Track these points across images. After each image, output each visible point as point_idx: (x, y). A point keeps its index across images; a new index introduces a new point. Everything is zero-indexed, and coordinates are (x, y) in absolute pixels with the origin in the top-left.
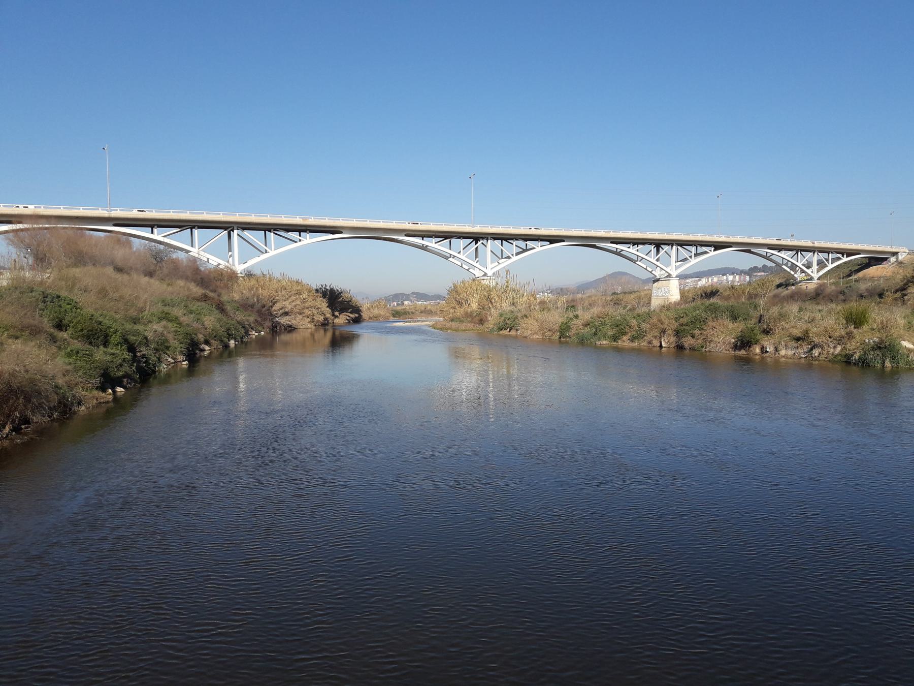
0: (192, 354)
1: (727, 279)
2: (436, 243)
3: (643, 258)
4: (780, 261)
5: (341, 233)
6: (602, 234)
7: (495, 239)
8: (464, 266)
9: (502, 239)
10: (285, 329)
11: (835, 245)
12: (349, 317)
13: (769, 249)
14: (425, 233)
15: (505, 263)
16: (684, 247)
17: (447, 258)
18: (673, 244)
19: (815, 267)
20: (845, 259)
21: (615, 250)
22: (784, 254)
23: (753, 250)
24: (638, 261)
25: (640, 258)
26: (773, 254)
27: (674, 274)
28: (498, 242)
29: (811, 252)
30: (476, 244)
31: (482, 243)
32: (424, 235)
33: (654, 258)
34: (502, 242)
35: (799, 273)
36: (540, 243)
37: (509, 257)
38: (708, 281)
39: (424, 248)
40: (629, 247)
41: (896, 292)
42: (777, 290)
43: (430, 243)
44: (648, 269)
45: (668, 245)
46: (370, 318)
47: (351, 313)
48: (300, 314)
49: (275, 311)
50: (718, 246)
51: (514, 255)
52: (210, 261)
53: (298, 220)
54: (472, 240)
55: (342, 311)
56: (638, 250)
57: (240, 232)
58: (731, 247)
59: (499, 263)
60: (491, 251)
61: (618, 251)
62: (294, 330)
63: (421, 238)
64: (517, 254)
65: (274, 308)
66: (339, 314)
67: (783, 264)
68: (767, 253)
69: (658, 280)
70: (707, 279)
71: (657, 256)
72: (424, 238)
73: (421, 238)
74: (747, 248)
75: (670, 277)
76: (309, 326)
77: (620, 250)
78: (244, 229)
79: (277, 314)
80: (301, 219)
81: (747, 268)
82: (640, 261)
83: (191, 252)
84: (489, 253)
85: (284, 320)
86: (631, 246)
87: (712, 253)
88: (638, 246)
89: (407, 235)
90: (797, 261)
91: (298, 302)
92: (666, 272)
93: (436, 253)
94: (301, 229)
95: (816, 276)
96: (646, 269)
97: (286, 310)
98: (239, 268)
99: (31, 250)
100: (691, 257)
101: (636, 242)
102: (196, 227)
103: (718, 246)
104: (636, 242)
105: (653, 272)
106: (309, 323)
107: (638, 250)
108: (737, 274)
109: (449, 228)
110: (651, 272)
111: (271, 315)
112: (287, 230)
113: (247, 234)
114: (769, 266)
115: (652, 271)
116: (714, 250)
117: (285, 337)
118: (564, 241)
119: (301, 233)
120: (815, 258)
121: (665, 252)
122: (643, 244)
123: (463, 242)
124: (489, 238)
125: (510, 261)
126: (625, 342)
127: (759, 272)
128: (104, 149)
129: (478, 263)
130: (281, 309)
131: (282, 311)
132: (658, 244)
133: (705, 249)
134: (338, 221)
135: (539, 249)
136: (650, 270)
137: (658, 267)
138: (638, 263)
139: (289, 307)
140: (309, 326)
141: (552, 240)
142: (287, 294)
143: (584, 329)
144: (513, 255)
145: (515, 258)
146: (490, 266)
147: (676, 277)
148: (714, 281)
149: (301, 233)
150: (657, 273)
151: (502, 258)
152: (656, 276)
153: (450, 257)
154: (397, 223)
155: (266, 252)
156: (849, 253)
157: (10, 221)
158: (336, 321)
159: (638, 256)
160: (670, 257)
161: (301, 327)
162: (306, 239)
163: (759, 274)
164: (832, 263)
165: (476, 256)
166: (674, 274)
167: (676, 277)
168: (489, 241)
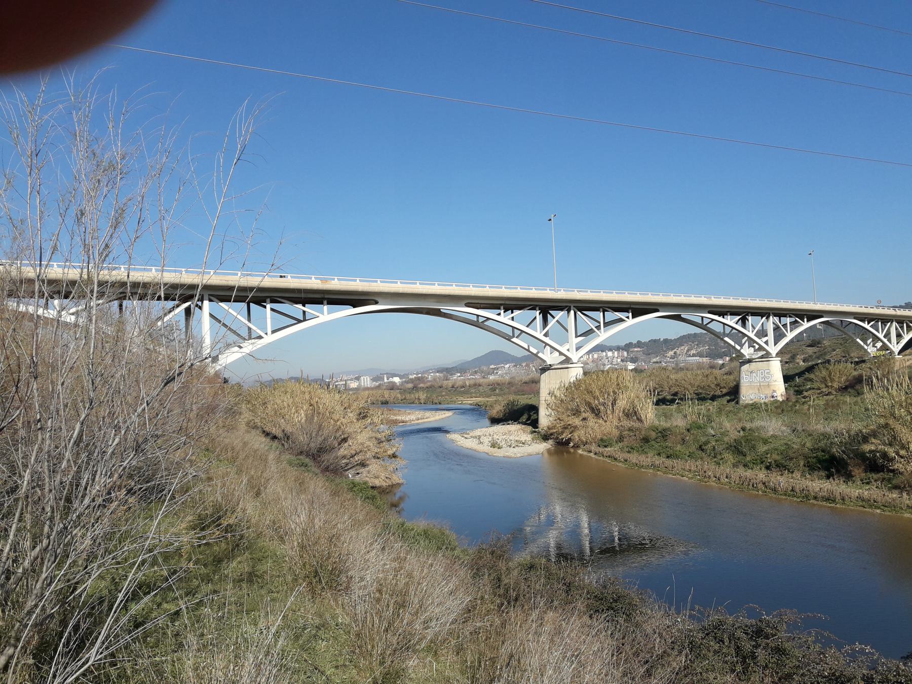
1: (606, 355)
3: (522, 331)
24: (513, 336)
25: (517, 332)
26: (488, 319)
28: (233, 311)
29: (562, 310)
33: (540, 333)
37: (260, 337)
38: (589, 358)
40: (499, 314)
50: (639, 309)
51: (269, 332)
53: (313, 283)
56: (513, 319)
57: (276, 306)
64: (273, 332)
67: (725, 335)
68: (702, 318)
71: (543, 330)
75: (568, 363)
80: (319, 281)
81: (623, 344)
82: (516, 337)
86: (502, 312)
88: (512, 313)
92: (561, 354)
100: (598, 328)
102: (325, 302)
103: (639, 309)
105: (540, 355)
108: (615, 351)
114: (662, 340)
115: (538, 353)
116: (633, 317)
120: (770, 323)
121: (557, 321)
127: (635, 348)
132: (546, 308)
136: (535, 351)
137: (548, 347)
138: (514, 340)
144: (266, 334)
151: (250, 338)
152: (544, 361)
155: (250, 335)
159: (513, 328)
160: (567, 330)
163: (636, 349)
164: (907, 334)
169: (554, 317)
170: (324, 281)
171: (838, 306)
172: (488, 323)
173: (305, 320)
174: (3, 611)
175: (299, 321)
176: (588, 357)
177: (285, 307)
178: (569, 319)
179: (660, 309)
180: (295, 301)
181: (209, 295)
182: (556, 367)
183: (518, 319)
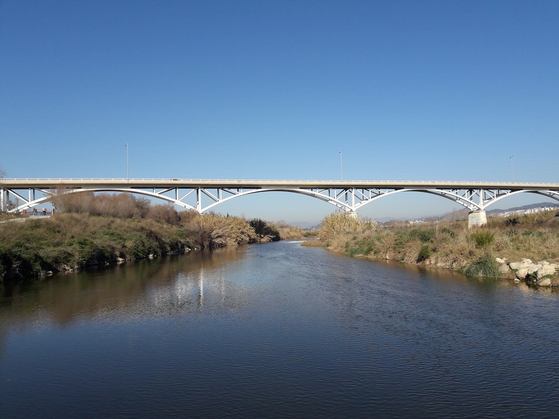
0: (102, 264)
2: (319, 192)
3: (460, 198)
5: (260, 188)
6: (430, 183)
7: (357, 188)
8: (338, 205)
9: (363, 189)
10: (219, 246)
12: (270, 237)
13: (550, 190)
14: (313, 187)
15: (364, 203)
16: (489, 190)
17: (327, 201)
18: (480, 189)
21: (441, 193)
23: (539, 191)
24: (457, 200)
25: (458, 199)
26: (554, 194)
27: (482, 208)
28: (360, 191)
30: (346, 191)
31: (349, 191)
32: (312, 187)
34: (498, 190)
36: (387, 190)
37: (367, 200)
38: (531, 211)
39: (313, 195)
40: (450, 192)
42: (555, 218)
43: (316, 192)
44: (465, 205)
45: (477, 189)
46: (287, 238)
47: (271, 235)
48: (229, 237)
49: (213, 235)
51: (370, 198)
52: (186, 207)
53: (235, 182)
54: (468, 190)
55: (265, 234)
57: (202, 190)
58: (522, 190)
59: (361, 203)
60: (355, 195)
61: (443, 194)
62: (225, 246)
64: (372, 198)
65: (212, 234)
66: (264, 236)
68: (550, 193)
69: (472, 212)
70: (530, 210)
72: (313, 190)
73: (311, 189)
74: (535, 190)
75: (480, 210)
76: (234, 244)
77: (444, 193)
78: (205, 188)
79: (214, 237)
82: (459, 200)
83: (175, 202)
84: (353, 196)
85: (218, 241)
87: (509, 194)
88: (457, 190)
89: (301, 188)
90: (176, 199)
91: (228, 230)
93: (453, 199)
96: (463, 205)
97: (219, 235)
98: (200, 210)
99: (54, 204)
101: (454, 188)
104: (454, 188)
105: (469, 207)
106: (234, 242)
107: (457, 192)
109: (298, 183)
110: (467, 207)
111: (211, 237)
112: (230, 188)
113: (206, 190)
115: (468, 206)
116: (510, 192)
117: (218, 251)
119: (239, 189)
121: (476, 193)
122: (460, 189)
123: (336, 192)
124: (353, 188)
125: (367, 202)
126: (371, 256)
128: (126, 146)
129: (347, 204)
131: (217, 235)
132: (471, 189)
133: (503, 191)
134: (299, 182)
136: (466, 206)
138: (457, 201)
139: (221, 233)
140: (234, 244)
141: (513, 189)
142: (222, 225)
143: (355, 246)
144: (369, 198)
145: (370, 200)
147: (484, 210)
148: (536, 211)
149: (239, 189)
150: (471, 208)
151: (363, 200)
152: (470, 210)
153: (329, 200)
154: (404, 182)
157: (48, 187)
158: (262, 240)
159: (457, 197)
160: (479, 196)
161: (229, 244)
162: (241, 193)
165: (346, 199)
167: (484, 210)
168: (353, 190)
169: (474, 192)
172: (445, 195)
173: (380, 194)
175: (378, 195)
176: (530, 212)
177: (374, 190)
179: (404, 188)
180: (377, 188)
181: (3, 188)
182: (475, 212)
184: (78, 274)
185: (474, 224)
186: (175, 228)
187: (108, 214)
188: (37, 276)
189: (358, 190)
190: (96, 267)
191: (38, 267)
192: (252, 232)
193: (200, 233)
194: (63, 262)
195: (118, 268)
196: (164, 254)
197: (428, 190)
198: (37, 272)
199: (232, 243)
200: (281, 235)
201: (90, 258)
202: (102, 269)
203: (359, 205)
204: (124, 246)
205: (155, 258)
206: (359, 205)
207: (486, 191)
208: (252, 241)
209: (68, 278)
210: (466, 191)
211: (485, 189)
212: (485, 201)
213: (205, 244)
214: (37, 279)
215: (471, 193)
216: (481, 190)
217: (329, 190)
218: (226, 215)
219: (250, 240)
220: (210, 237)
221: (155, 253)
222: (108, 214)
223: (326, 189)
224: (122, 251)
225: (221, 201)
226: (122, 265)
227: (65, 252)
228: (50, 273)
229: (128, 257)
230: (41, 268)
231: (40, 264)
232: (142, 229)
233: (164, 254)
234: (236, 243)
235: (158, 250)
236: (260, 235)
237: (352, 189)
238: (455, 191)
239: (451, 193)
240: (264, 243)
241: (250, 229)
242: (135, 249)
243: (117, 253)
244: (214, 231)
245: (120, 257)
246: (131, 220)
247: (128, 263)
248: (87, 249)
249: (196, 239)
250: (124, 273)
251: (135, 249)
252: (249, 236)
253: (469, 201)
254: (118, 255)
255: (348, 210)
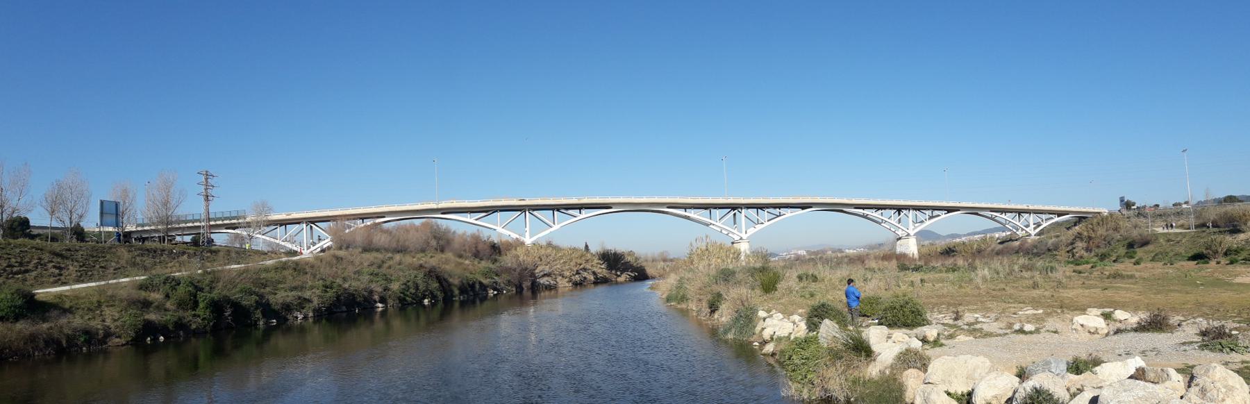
4: (1004, 221)
6: (434, 206)
7: (748, 208)
8: (723, 231)
9: (757, 208)
11: (1047, 208)
12: (629, 275)
15: (759, 227)
19: (1032, 226)
20: (1057, 219)
22: (470, 218)
27: (912, 233)
28: (752, 212)
32: (686, 207)
35: (1020, 230)
36: (789, 210)
37: (762, 223)
39: (865, 217)
41: (1067, 246)
43: (692, 213)
44: (892, 229)
45: (906, 209)
47: (631, 272)
60: (745, 216)
63: (684, 210)
64: (768, 221)
65: (536, 271)
69: (900, 239)
74: (974, 211)
76: (567, 285)
78: (534, 210)
84: (743, 218)
85: (544, 281)
87: (943, 215)
94: (580, 207)
95: (1033, 233)
98: (528, 241)
113: (535, 213)
118: (811, 207)
120: (1032, 219)
122: (885, 209)
123: (717, 213)
125: (763, 226)
130: (541, 271)
131: (542, 273)
132: (899, 209)
135: (943, 216)
136: (894, 230)
138: (883, 224)
139: (547, 269)
144: (926, 220)
145: (767, 224)
146: (911, 226)
150: (900, 233)
156: (1060, 214)
158: (619, 279)
165: (735, 223)
166: (912, 233)
170: (579, 199)
171: (515, 201)
173: (780, 216)
174: (216, 402)
175: (778, 216)
177: (771, 210)
178: (911, 213)
180: (775, 208)
183: (1008, 217)
184: (315, 322)
185: (799, 252)
186: (485, 264)
187: (387, 250)
188: (256, 324)
189: (749, 210)
190: (344, 315)
191: (258, 314)
192: (602, 270)
193: (518, 270)
194: (296, 309)
195: (377, 317)
196: (448, 300)
197: (845, 209)
198: (256, 322)
199: (563, 284)
200: (650, 271)
201: (331, 304)
202: (352, 320)
203: (751, 231)
204: (386, 289)
205: (433, 305)
206: (751, 231)
207: (918, 213)
208: (600, 281)
209: (302, 330)
210: (893, 211)
211: (916, 210)
212: (916, 225)
213: (524, 286)
214: (256, 328)
215: (899, 214)
216: (911, 211)
217: (113, 214)
218: (583, 247)
219: (596, 278)
220: (533, 275)
221: (433, 297)
222: (387, 250)
223: (706, 209)
224: (382, 295)
225: (556, 227)
226: (384, 313)
227: (300, 298)
228: (273, 322)
229: (390, 302)
230: (261, 317)
231: (261, 311)
232: (421, 266)
233: (448, 300)
234: (571, 284)
235: (439, 293)
236: (616, 272)
237: (742, 209)
238: (880, 212)
239: (875, 214)
240: (621, 283)
241: (597, 263)
242: (401, 293)
243: (376, 297)
244: (539, 267)
245: (380, 302)
246: (423, 255)
247: (391, 309)
248: (330, 293)
249: (509, 278)
250: (387, 323)
251: (401, 293)
252: (594, 273)
253: (897, 225)
254: (377, 300)
255: (737, 238)
